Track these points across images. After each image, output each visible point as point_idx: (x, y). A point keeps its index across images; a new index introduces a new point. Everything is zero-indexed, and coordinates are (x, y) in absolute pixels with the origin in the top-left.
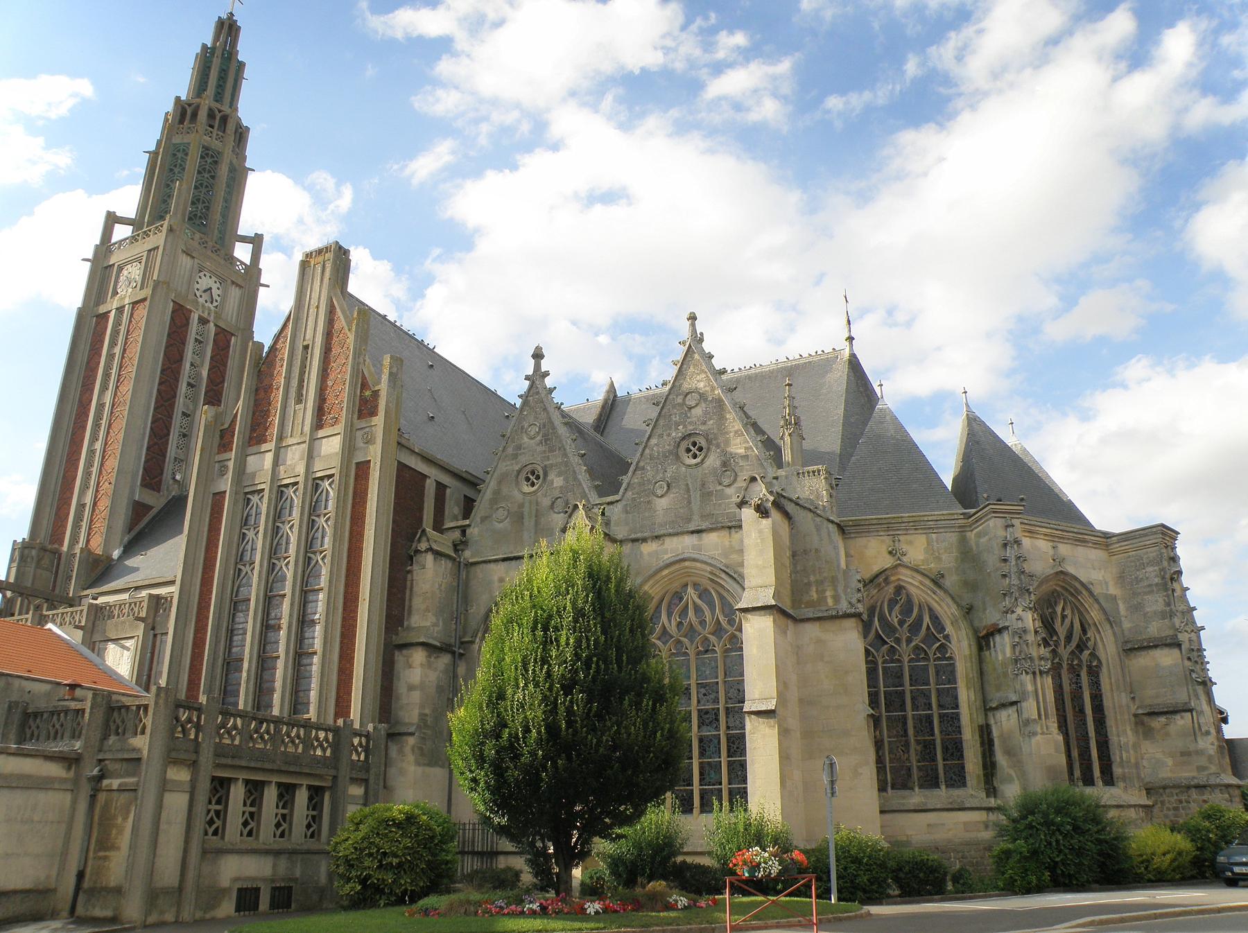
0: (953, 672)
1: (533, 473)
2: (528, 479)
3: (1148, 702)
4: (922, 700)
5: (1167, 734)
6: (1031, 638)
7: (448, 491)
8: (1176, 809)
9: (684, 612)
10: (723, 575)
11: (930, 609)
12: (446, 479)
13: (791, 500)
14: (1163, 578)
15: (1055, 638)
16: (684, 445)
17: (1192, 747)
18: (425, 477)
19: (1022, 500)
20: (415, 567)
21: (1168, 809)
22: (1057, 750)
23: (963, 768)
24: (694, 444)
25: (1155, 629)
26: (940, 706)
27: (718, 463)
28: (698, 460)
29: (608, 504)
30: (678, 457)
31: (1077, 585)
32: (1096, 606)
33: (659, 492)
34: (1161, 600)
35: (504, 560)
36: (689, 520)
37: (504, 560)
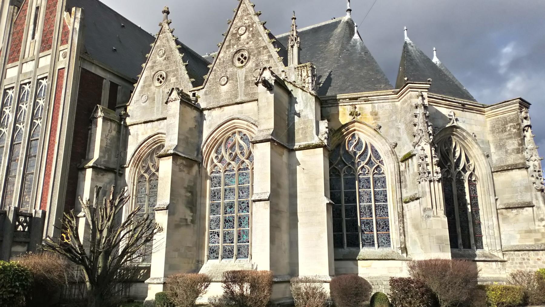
0: (384, 182)
1: (161, 76)
2: (158, 79)
3: (506, 202)
4: (366, 197)
5: (517, 220)
6: (429, 160)
7: (119, 87)
8: (521, 263)
9: (233, 147)
10: (253, 126)
11: (372, 147)
12: (116, 81)
13: (291, 83)
14: (519, 129)
15: (449, 164)
16: (238, 56)
17: (532, 228)
18: (103, 79)
19: (429, 81)
20: (93, 127)
21: (516, 263)
22: (444, 227)
23: (389, 236)
24: (242, 55)
25: (512, 160)
26: (376, 201)
27: (254, 65)
28: (244, 64)
29: (197, 90)
30: (233, 62)
31: (464, 134)
32: (476, 146)
33: (223, 83)
34: (516, 142)
35: (145, 122)
36: (237, 97)
37: (145, 122)
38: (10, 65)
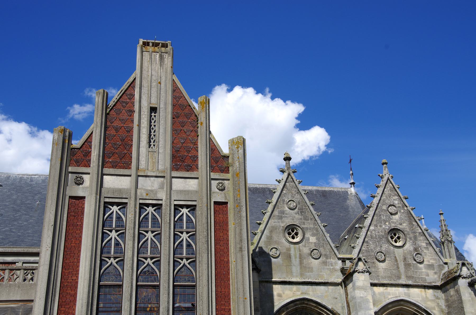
36: (399, 278)
38: (112, 171)
